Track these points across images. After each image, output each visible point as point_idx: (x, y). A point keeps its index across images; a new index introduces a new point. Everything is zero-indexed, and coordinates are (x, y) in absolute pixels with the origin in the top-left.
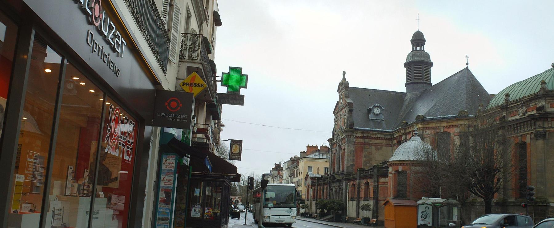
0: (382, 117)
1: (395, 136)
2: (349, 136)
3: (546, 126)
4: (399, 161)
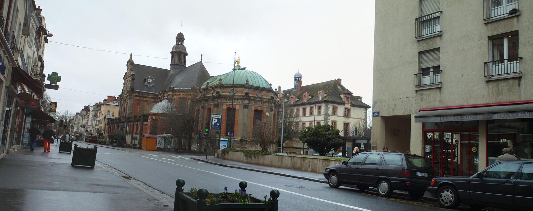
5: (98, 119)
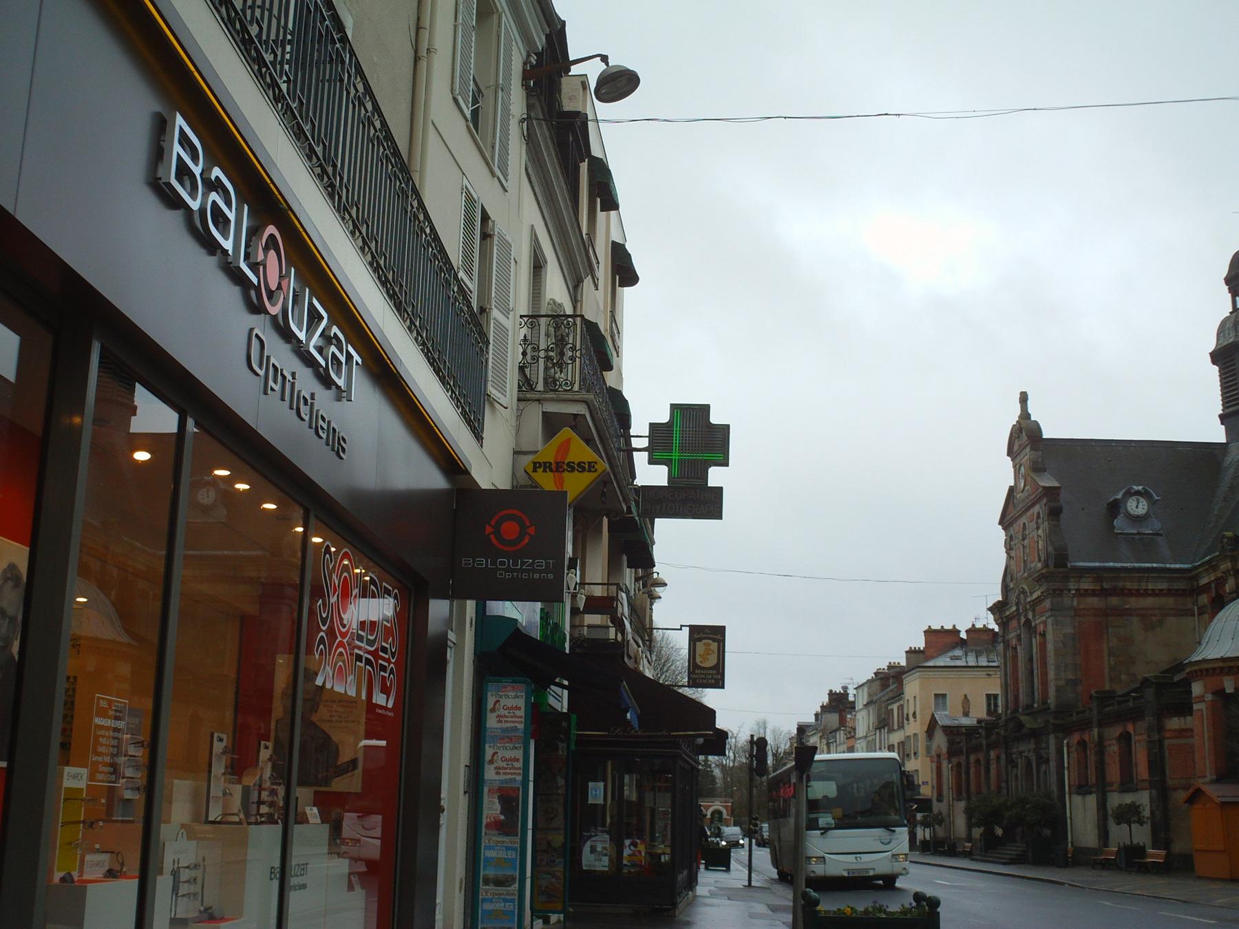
4: (1223, 660)
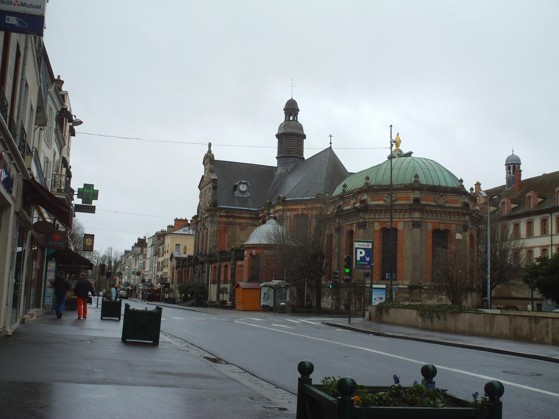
0: (248, 194)
1: (261, 215)
2: (212, 216)
3: (366, 217)
4: (253, 244)
5: (161, 259)
